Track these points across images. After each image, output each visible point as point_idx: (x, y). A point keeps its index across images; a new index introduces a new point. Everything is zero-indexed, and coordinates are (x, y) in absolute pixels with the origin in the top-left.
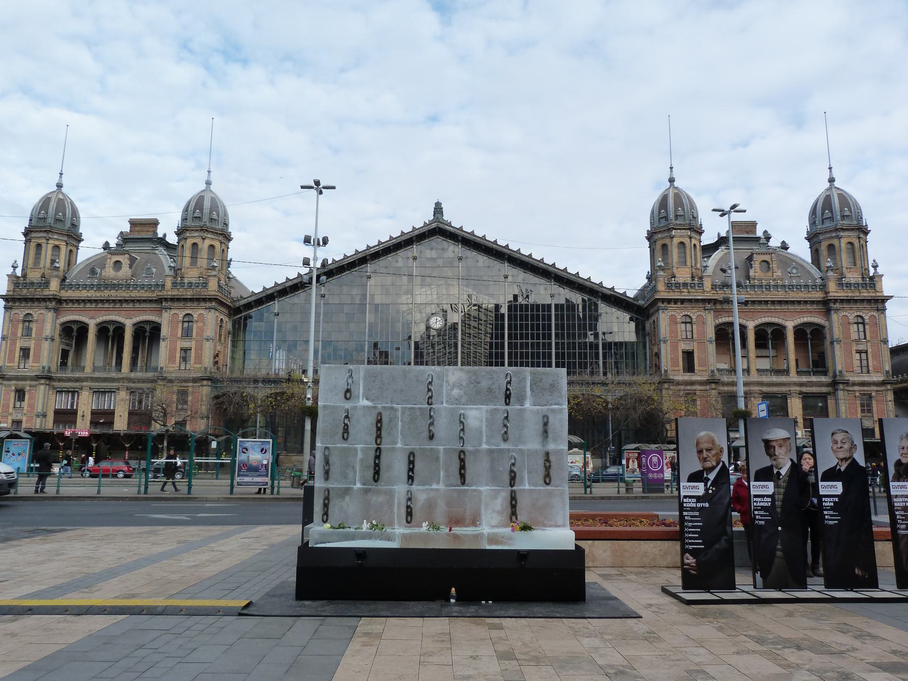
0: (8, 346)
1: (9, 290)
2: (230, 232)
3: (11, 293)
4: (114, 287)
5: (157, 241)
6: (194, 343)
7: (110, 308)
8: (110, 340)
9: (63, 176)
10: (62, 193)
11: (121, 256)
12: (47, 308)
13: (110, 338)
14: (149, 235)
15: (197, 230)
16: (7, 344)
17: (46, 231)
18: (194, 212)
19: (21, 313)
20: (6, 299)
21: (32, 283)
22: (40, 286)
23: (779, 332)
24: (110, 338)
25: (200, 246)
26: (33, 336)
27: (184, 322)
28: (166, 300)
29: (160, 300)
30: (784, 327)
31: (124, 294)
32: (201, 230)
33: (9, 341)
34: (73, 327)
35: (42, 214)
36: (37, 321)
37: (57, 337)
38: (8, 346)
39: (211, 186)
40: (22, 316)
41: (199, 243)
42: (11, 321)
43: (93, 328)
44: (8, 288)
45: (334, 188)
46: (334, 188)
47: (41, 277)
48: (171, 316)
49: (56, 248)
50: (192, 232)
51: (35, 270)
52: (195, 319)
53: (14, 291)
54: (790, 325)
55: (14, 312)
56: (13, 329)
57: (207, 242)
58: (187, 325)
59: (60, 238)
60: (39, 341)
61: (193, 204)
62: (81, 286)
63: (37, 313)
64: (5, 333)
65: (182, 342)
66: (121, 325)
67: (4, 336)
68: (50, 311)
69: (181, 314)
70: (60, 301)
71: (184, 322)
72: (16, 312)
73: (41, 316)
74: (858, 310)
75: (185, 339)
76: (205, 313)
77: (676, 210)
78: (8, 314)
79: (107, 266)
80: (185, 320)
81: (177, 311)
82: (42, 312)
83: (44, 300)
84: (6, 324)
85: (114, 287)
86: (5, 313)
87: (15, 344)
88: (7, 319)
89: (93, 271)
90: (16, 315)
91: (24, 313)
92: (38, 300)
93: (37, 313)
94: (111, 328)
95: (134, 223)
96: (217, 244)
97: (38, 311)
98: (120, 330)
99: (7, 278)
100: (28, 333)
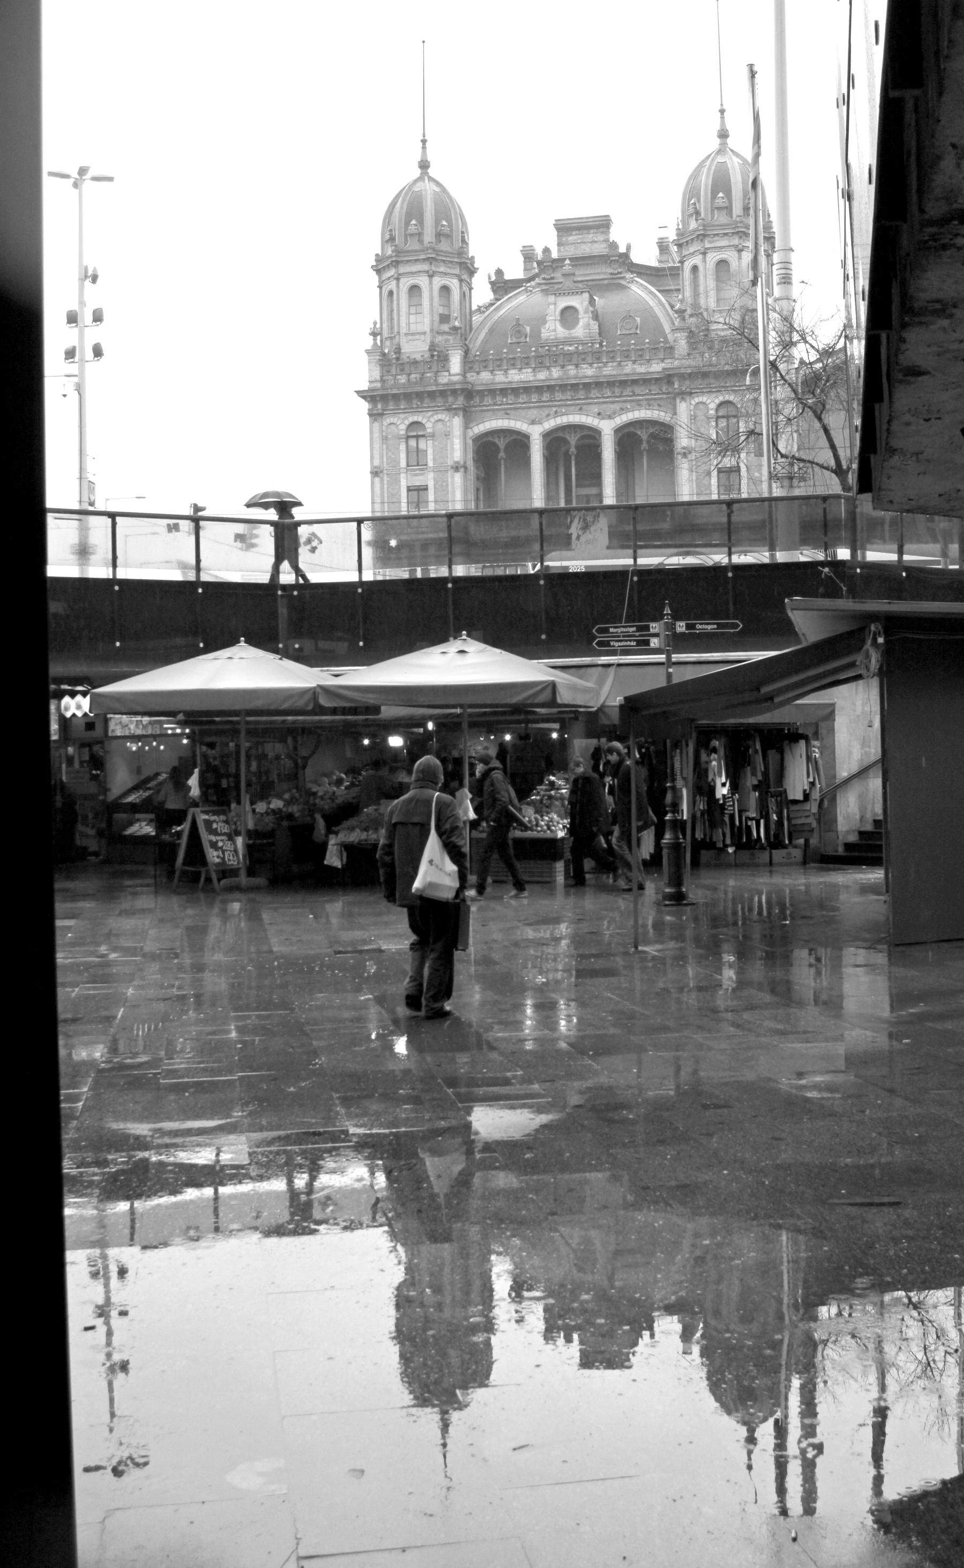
0: (386, 486)
1: (373, 379)
2: (473, 257)
3: (379, 385)
4: (567, 359)
5: (617, 261)
6: (431, 476)
7: (567, 400)
8: (573, 463)
9: (427, 144)
10: (431, 179)
11: (574, 297)
12: (449, 409)
13: (573, 458)
14: (599, 249)
15: (726, 234)
16: (382, 480)
17: (428, 258)
18: (407, 224)
19: (400, 422)
20: (371, 397)
21: (415, 363)
22: (430, 368)
23: (520, 443)
24: (573, 458)
25: (734, 264)
26: (430, 464)
27: (718, 418)
28: (682, 377)
29: (667, 378)
30: (527, 437)
31: (641, 369)
32: (733, 233)
33: (385, 477)
34: (497, 441)
35: (720, 201)
36: (433, 436)
37: (470, 464)
38: (386, 486)
39: (429, 171)
40: (403, 427)
41: (730, 260)
42: (385, 439)
43: (538, 442)
44: (370, 376)
45: (110, 179)
46: (110, 179)
47: (430, 350)
48: (692, 407)
49: (414, 290)
50: (716, 238)
51: (414, 337)
52: (429, 430)
53: (382, 380)
54: (607, 429)
55: (387, 420)
56: (390, 454)
57: (438, 282)
58: (725, 424)
59: (449, 271)
60: (440, 470)
61: (705, 181)
62: (505, 361)
63: (430, 420)
64: (376, 463)
65: (409, 476)
66: (519, 437)
67: (376, 467)
68: (456, 414)
69: (712, 402)
70: (469, 393)
71: (718, 418)
72: (392, 420)
73: (440, 425)
74: (411, 410)
75: (415, 470)
76: (709, 401)
77: (437, 222)
78: (376, 425)
79: (548, 318)
80: (720, 414)
81: (704, 399)
82: (439, 416)
83: (443, 393)
84: (377, 446)
85: (567, 359)
86: (371, 423)
87: (398, 481)
88: (376, 435)
89: (519, 332)
90: (392, 426)
91: (407, 422)
92: (432, 395)
93: (432, 420)
94: (573, 440)
95: (564, 228)
96: (454, 284)
97: (432, 416)
98: (590, 439)
99: (366, 357)
100: (417, 460)
